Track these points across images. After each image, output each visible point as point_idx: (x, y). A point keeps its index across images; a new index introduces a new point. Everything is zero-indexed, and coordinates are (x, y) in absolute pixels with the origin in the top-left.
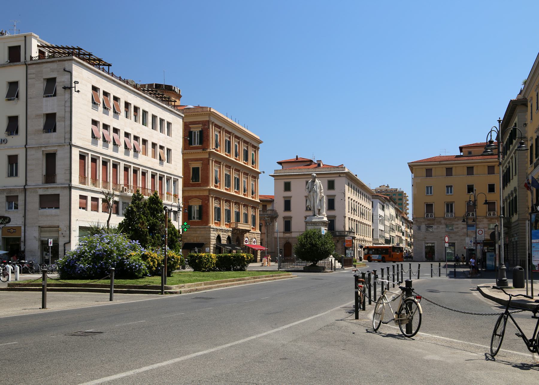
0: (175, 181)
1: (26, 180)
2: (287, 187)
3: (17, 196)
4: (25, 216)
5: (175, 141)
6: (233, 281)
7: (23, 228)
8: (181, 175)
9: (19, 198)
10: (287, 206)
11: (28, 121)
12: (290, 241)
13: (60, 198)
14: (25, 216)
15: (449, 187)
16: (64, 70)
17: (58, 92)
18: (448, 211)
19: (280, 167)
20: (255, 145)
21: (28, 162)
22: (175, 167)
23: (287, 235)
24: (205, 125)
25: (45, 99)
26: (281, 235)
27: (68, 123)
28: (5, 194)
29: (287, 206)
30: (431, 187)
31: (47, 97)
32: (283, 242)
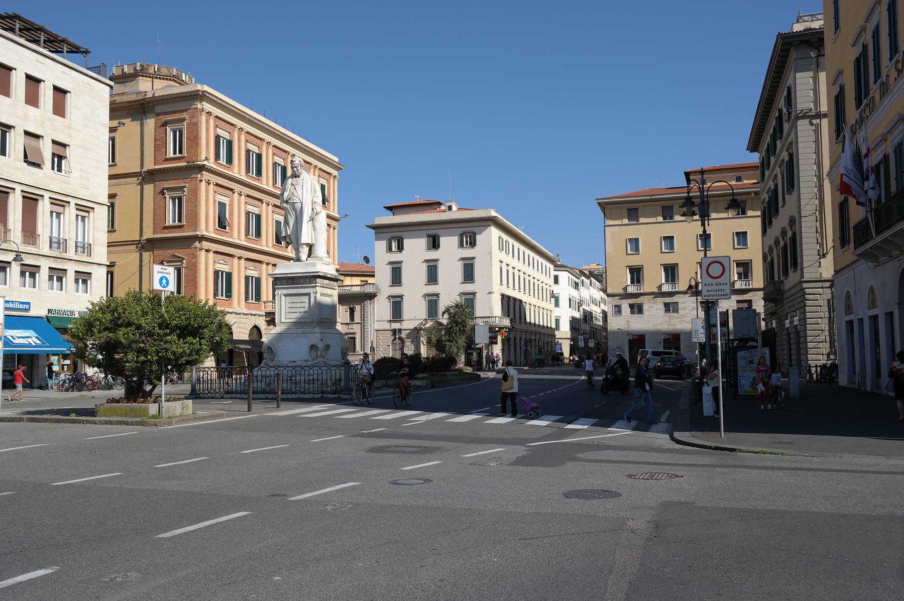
10: (397, 277)
26: (387, 326)
29: (397, 277)
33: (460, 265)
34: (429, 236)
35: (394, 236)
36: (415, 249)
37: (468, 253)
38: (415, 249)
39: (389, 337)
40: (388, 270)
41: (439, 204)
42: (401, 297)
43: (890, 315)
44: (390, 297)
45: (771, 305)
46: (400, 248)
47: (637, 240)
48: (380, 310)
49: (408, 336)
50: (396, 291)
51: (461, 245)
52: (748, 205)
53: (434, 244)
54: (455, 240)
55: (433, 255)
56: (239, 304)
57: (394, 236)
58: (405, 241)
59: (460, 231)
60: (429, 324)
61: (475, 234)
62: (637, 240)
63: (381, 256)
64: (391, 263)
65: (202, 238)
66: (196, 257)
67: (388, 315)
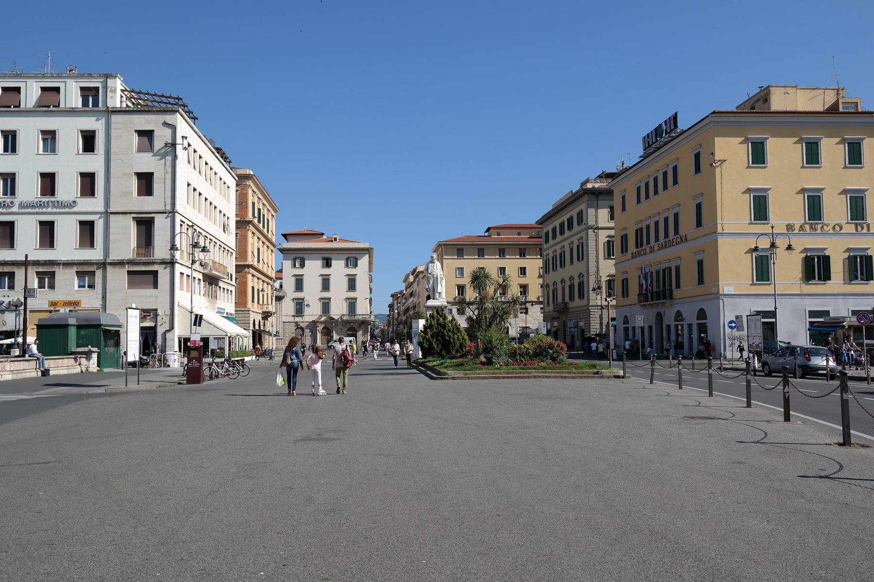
4: (104, 297)
14: (104, 297)
26: (292, 319)
29: (299, 285)
33: (346, 279)
34: (324, 259)
35: (299, 257)
36: (313, 269)
37: (351, 271)
38: (313, 269)
39: (293, 327)
40: (293, 281)
41: (323, 234)
42: (356, 299)
43: (650, 327)
44: (294, 299)
45: (714, 290)
46: (302, 266)
47: (462, 269)
48: (288, 307)
49: (307, 327)
50: (299, 295)
51: (347, 266)
52: (527, 251)
53: (328, 263)
54: (343, 263)
55: (326, 271)
56: (253, 302)
57: (299, 257)
58: (306, 262)
59: (346, 256)
60: (323, 319)
61: (356, 259)
62: (462, 269)
63: (289, 271)
64: (295, 275)
65: (249, 266)
66: (246, 278)
67: (292, 312)
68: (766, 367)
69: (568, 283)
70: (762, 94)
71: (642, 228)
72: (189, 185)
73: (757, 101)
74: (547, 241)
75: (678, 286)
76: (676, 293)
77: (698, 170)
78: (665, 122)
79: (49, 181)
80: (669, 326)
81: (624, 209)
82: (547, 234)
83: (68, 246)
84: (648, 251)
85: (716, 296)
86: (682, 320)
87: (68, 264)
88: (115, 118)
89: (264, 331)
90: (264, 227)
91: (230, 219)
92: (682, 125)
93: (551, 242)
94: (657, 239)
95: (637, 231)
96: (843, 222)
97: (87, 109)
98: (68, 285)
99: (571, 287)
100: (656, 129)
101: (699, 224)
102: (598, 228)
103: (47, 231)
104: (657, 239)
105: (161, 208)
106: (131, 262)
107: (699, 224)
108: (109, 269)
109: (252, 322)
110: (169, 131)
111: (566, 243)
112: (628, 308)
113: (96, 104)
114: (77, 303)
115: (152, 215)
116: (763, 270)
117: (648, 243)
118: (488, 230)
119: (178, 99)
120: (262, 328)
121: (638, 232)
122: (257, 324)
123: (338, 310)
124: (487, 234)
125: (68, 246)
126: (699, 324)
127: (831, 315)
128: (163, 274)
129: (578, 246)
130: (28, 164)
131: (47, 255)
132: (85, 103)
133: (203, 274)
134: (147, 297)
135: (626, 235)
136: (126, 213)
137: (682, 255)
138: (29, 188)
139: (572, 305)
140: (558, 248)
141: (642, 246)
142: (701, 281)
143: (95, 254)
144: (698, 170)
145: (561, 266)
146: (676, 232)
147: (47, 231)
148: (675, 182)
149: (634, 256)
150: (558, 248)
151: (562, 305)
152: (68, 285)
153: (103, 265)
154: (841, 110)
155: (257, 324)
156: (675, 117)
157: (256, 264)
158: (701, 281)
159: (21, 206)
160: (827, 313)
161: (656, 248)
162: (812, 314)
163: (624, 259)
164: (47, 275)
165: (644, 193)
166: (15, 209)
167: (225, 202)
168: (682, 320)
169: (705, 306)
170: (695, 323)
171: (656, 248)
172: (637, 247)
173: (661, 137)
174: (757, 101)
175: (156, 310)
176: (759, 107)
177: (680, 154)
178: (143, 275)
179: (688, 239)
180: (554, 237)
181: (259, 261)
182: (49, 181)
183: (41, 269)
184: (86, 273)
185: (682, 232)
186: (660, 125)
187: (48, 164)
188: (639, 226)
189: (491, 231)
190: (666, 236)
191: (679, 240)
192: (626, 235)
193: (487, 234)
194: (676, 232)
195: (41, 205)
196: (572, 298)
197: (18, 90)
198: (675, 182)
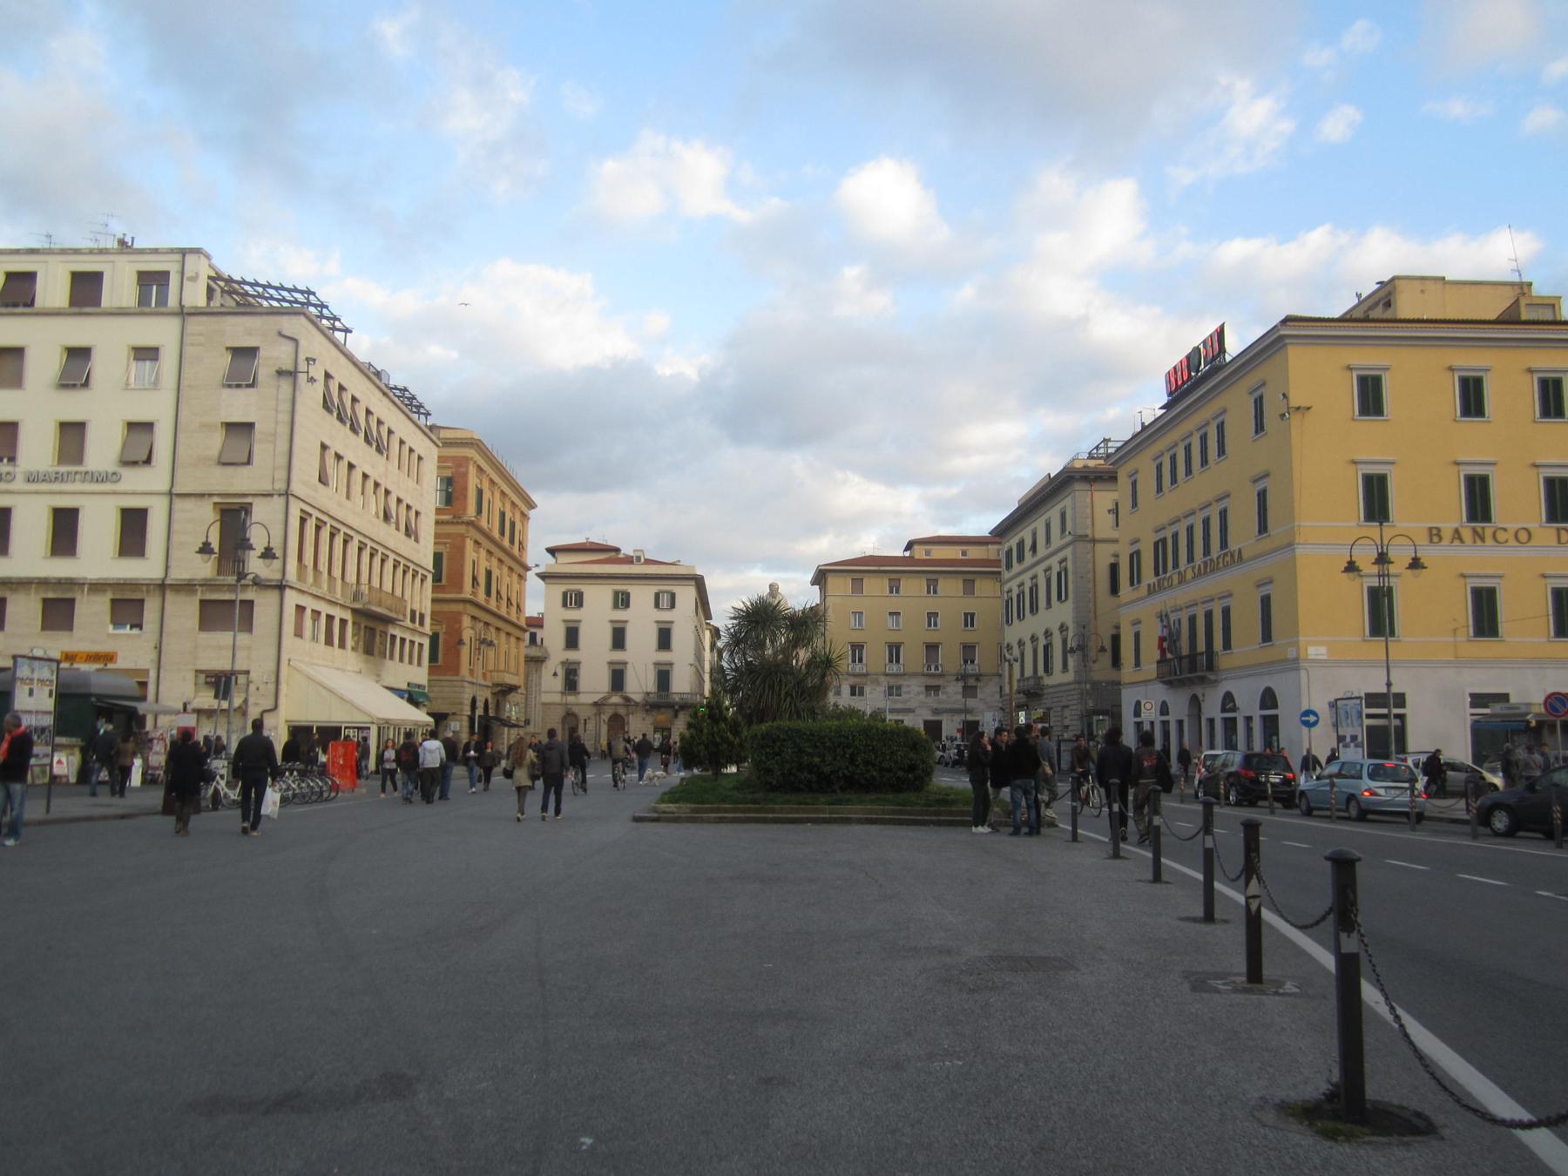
0: (424, 579)
1: (167, 567)
2: (574, 600)
3: (142, 601)
4: (159, 649)
5: (426, 497)
6: (749, 811)
7: (153, 674)
8: (431, 568)
9: (147, 606)
10: (572, 638)
11: (181, 436)
12: (576, 710)
13: (256, 609)
14: (159, 649)
15: (932, 616)
16: (281, 334)
17: (260, 378)
18: (891, 661)
19: (549, 559)
20: (524, 508)
21: (175, 527)
22: (423, 552)
23: (571, 699)
24: (459, 465)
25: (228, 391)
26: (557, 698)
27: (283, 446)
28: (109, 596)
29: (572, 638)
30: (972, 615)
31: (230, 386)
32: (560, 712)
45: (1291, 654)
68: (1353, 803)
69: (1042, 642)
70: (1382, 294)
71: (1164, 540)
72: (324, 447)
73: (1376, 304)
74: (1009, 566)
75: (1227, 645)
76: (1224, 661)
77: (1259, 427)
78: (1204, 342)
79: (72, 434)
80: (1211, 721)
81: (1135, 504)
82: (1009, 552)
83: (97, 555)
84: (1176, 581)
85: (1293, 664)
86: (1234, 709)
87: (97, 587)
88: (192, 320)
89: (497, 719)
90: (502, 533)
91: (422, 518)
92: (1234, 346)
93: (1016, 567)
94: (1191, 559)
95: (1156, 544)
96: (1532, 526)
97: (146, 310)
98: (93, 625)
99: (1047, 648)
100: (1188, 357)
101: (1263, 528)
102: (1094, 541)
103: (65, 530)
104: (1191, 559)
105: (266, 487)
106: (208, 585)
107: (1263, 528)
108: (169, 596)
109: (468, 702)
110: (288, 347)
111: (1040, 570)
112: (1142, 689)
113: (162, 301)
114: (109, 657)
115: (249, 500)
116: (1381, 614)
117: (1176, 565)
118: (910, 546)
119: (309, 292)
120: (491, 713)
121: (1159, 546)
122: (480, 705)
123: (640, 683)
124: (907, 554)
125: (97, 555)
126: (1264, 718)
127: (1513, 700)
128: (264, 605)
129: (1059, 575)
130: (35, 407)
131: (62, 568)
132: (143, 300)
133: (355, 611)
134: (216, 650)
135: (1138, 553)
136: (202, 495)
137: (1236, 587)
138: (38, 448)
139: (1048, 681)
140: (1026, 578)
141: (1165, 571)
142: (1267, 636)
143: (146, 569)
144: (1259, 427)
145: (1031, 611)
146: (1224, 544)
147: (65, 530)
148: (1222, 451)
149: (1151, 591)
150: (1026, 578)
151: (1032, 682)
152: (93, 625)
153: (162, 587)
154: (1524, 317)
155: (480, 705)
156: (1220, 333)
157: (481, 597)
158: (1267, 636)
159: (31, 479)
160: (1504, 697)
161: (1189, 575)
162: (1478, 700)
163: (1135, 595)
164: (59, 610)
165: (1168, 476)
166: (19, 484)
167: (411, 483)
168: (1234, 709)
169: (1278, 684)
170: (1257, 714)
171: (1189, 575)
172: (1157, 574)
173: (1200, 377)
174: (1376, 304)
175: (248, 672)
176: (1378, 313)
177: (1236, 404)
178: (220, 613)
179: (1245, 556)
180: (1021, 559)
181: (488, 593)
182: (72, 434)
183: (51, 595)
184: (127, 606)
185: (1233, 546)
186: (1197, 349)
187: (72, 406)
188: (1161, 535)
189: (916, 547)
190: (1207, 552)
191: (1228, 559)
192: (1138, 553)
193: (907, 554)
194: (1224, 544)
195: (59, 478)
196: (1047, 669)
197: (31, 276)
198: (1222, 451)
